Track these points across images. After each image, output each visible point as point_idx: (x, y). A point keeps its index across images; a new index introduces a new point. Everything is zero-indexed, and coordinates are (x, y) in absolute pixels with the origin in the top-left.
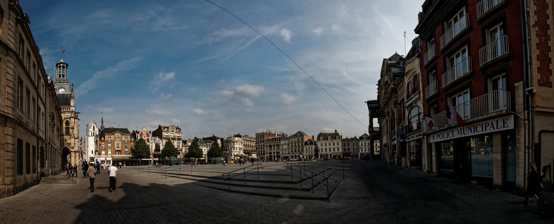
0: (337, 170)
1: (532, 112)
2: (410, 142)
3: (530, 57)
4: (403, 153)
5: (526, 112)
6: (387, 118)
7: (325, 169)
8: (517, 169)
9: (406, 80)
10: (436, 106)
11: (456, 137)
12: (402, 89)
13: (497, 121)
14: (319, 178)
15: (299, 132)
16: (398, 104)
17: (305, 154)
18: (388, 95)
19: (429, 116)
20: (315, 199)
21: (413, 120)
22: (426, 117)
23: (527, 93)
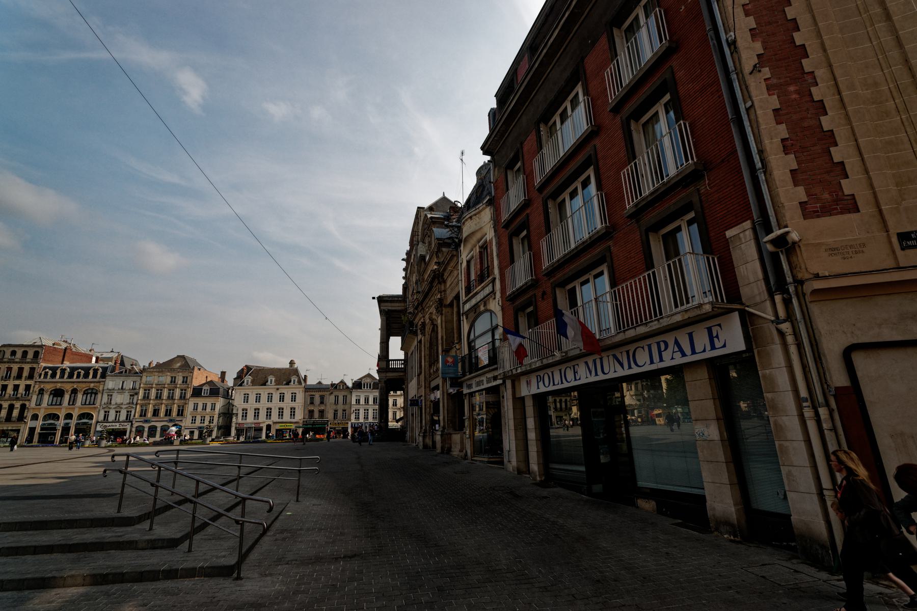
0: (282, 472)
1: (801, 296)
2: (471, 395)
3: (761, 152)
4: (457, 422)
5: (778, 298)
6: (420, 337)
7: (244, 471)
8: (784, 470)
9: (465, 254)
10: (531, 309)
11: (583, 381)
12: (456, 272)
13: (691, 335)
14: (220, 500)
15: (182, 358)
16: (446, 306)
17: (187, 422)
18: (424, 286)
19: (516, 333)
20: (191, 573)
21: (478, 343)
22: (509, 336)
23: (770, 247)
